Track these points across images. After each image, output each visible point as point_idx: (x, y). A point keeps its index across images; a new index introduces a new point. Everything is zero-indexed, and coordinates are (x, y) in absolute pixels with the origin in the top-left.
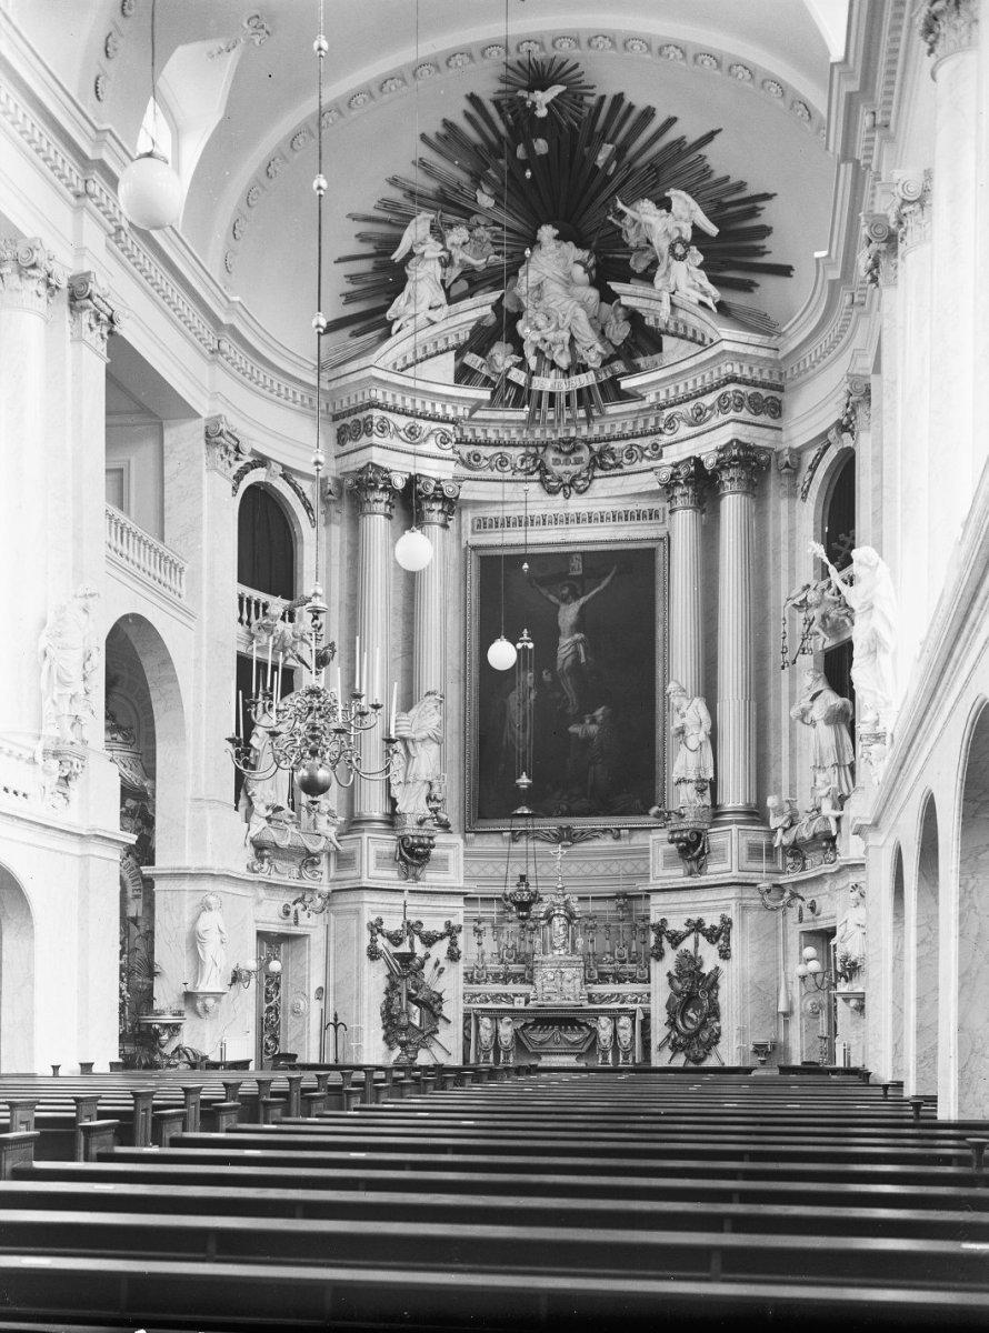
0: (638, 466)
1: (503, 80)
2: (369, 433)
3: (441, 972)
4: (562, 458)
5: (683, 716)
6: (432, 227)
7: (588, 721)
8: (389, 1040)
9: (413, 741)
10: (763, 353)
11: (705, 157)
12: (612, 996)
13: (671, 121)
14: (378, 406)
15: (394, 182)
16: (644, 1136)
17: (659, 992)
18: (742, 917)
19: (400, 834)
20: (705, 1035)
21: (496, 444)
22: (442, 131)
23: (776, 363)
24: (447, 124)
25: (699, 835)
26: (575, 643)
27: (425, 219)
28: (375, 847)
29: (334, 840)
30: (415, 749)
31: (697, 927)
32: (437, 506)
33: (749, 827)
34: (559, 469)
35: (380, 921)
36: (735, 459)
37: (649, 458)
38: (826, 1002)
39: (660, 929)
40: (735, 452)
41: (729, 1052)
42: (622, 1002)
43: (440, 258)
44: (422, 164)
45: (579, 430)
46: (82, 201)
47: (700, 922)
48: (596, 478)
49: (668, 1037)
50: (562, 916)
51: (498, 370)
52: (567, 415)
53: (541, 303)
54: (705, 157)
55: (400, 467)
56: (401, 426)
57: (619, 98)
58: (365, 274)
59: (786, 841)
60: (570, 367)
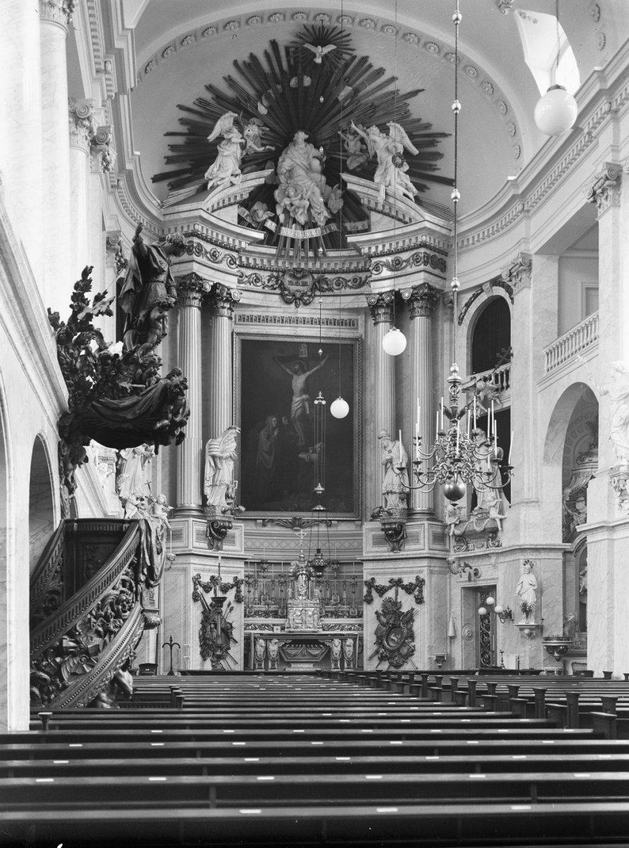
0: (343, 291)
1: (298, 36)
2: (190, 252)
3: (231, 609)
4: (294, 281)
5: (390, 452)
6: (234, 120)
7: (311, 451)
8: (204, 655)
9: (220, 458)
10: (444, 231)
11: (408, 105)
12: (336, 625)
13: (393, 79)
14: (198, 236)
15: (210, 88)
16: (248, 715)
17: (370, 625)
18: (430, 578)
19: (211, 519)
20: (404, 651)
21: (253, 268)
22: (248, 60)
23: (447, 238)
24: (252, 57)
25: (402, 527)
26: (303, 401)
27: (231, 116)
28: (195, 527)
29: (167, 521)
30: (222, 463)
31: (397, 583)
32: (227, 305)
33: (434, 523)
34: (293, 288)
35: (373, 579)
36: (425, 295)
37: (351, 287)
38: (474, 630)
39: (370, 584)
40: (426, 291)
41: (421, 661)
42: (342, 630)
43: (240, 144)
44: (229, 80)
45: (306, 264)
46: (100, 75)
47: (400, 581)
48: (316, 296)
49: (377, 652)
50: (305, 574)
51: (259, 220)
52: (302, 254)
53: (292, 181)
54: (408, 105)
55: (210, 276)
56: (208, 250)
57: (365, 59)
58: (180, 146)
59: (458, 532)
60: (306, 223)
